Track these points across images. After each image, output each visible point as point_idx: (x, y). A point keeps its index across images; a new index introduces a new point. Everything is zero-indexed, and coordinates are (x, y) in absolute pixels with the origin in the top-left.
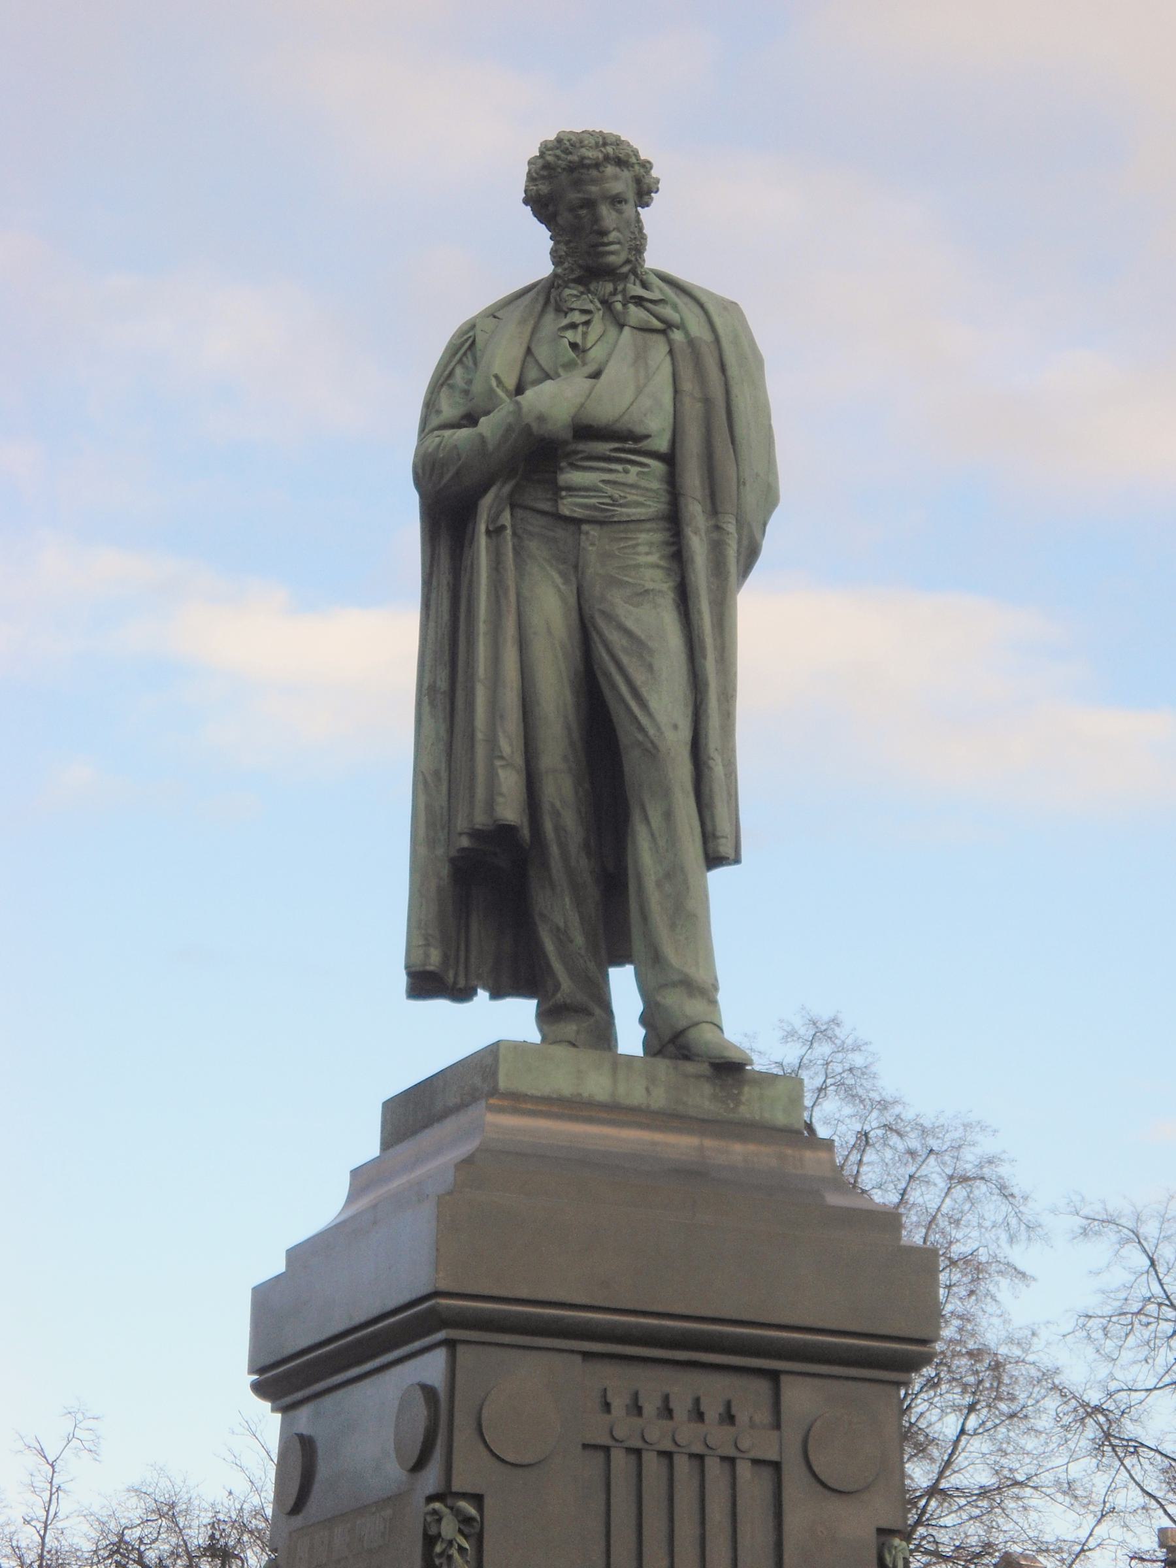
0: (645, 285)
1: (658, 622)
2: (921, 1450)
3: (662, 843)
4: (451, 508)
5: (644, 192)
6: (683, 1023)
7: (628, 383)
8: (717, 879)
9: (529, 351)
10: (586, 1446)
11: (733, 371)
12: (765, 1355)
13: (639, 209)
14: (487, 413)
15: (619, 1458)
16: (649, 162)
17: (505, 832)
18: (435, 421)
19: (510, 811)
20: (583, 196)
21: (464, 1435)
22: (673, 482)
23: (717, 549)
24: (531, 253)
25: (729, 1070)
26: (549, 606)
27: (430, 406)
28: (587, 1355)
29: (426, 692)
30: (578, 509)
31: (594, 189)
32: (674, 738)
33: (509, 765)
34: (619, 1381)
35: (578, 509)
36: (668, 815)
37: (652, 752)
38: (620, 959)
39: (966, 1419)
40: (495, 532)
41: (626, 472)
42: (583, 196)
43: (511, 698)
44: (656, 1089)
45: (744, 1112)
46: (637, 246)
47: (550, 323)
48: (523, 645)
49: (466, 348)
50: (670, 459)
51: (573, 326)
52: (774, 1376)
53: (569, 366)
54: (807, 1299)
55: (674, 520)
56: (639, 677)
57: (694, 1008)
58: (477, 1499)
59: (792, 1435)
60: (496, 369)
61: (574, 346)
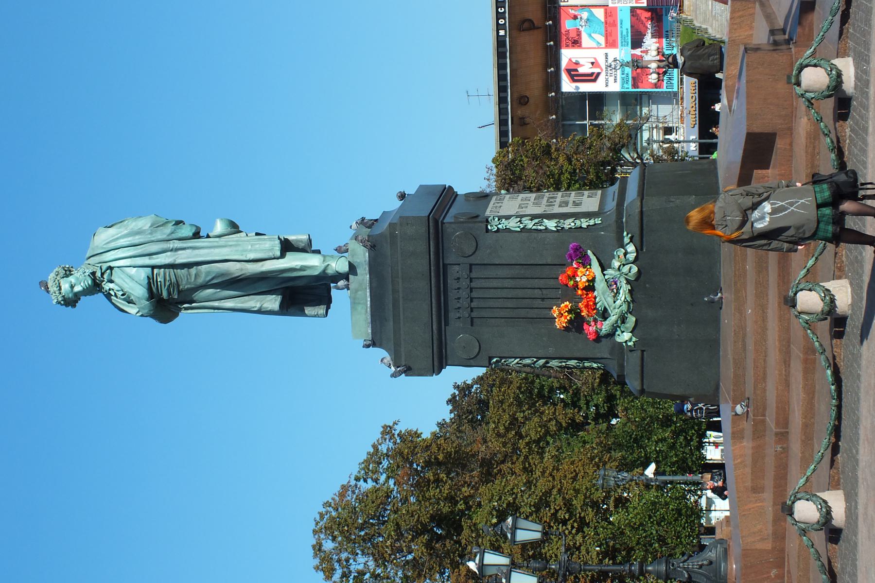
10: (472, 325)
28: (447, 324)
34: (452, 315)
50: (153, 267)
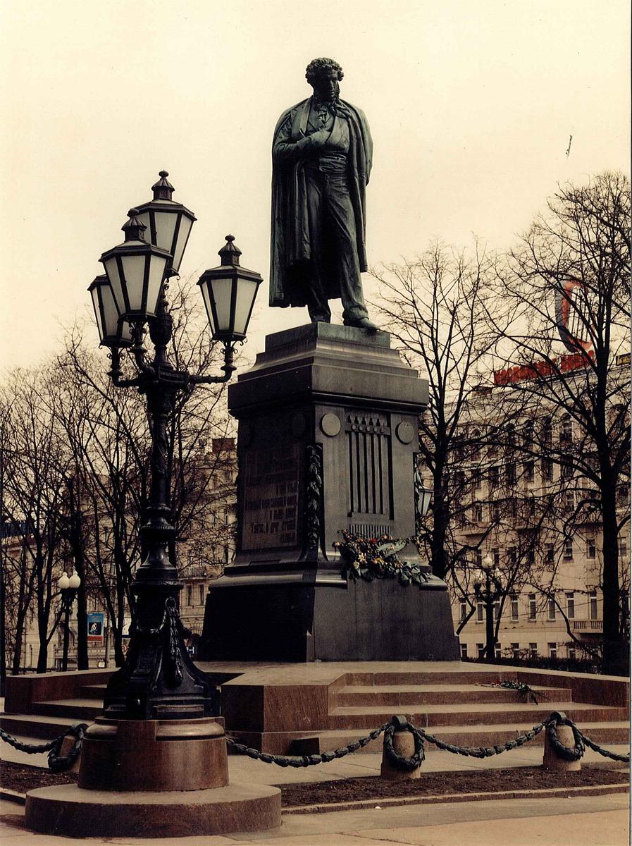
0: (340, 104)
1: (347, 203)
3: (350, 266)
5: (340, 77)
6: (359, 318)
8: (362, 275)
9: (308, 122)
11: (365, 130)
14: (299, 140)
15: (353, 434)
16: (337, 68)
18: (279, 140)
20: (323, 76)
24: (308, 91)
26: (315, 196)
27: (276, 135)
31: (329, 76)
32: (353, 238)
33: (306, 243)
36: (352, 259)
37: (348, 241)
40: (300, 175)
41: (338, 159)
42: (323, 76)
45: (376, 343)
47: (314, 114)
49: (287, 121)
51: (322, 115)
53: (322, 127)
56: (343, 220)
57: (362, 313)
59: (393, 428)
60: (301, 127)
61: (323, 121)
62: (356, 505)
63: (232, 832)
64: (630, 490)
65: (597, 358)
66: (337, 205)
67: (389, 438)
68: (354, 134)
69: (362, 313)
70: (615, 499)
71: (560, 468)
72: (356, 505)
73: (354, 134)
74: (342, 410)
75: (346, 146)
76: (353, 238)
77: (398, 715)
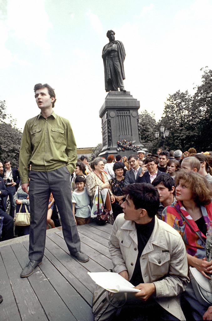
1: (118, 63)
2: (186, 288)
4: (104, 57)
5: (114, 34)
7: (114, 46)
12: (128, 109)
13: (190, 268)
17: (110, 79)
19: (110, 78)
20: (110, 35)
21: (109, 116)
22: (118, 54)
23: (122, 59)
24: (107, 41)
25: (125, 91)
29: (105, 72)
30: (113, 56)
32: (120, 71)
35: (113, 56)
37: (119, 72)
38: (118, 87)
39: (127, 247)
40: (107, 60)
42: (110, 35)
43: (109, 70)
44: (121, 92)
46: (114, 38)
48: (110, 67)
50: (118, 52)
52: (129, 110)
54: (131, 105)
55: (118, 56)
56: (117, 67)
58: (110, 120)
62: (121, 133)
63: (89, 223)
64: (208, 224)
65: (208, 151)
66: (116, 64)
67: (130, 116)
68: (118, 46)
69: (123, 88)
70: (13, 179)
71: (164, 117)
72: (121, 133)
73: (118, 46)
74: (115, 111)
75: (117, 50)
76: (120, 71)
77: (69, 255)
